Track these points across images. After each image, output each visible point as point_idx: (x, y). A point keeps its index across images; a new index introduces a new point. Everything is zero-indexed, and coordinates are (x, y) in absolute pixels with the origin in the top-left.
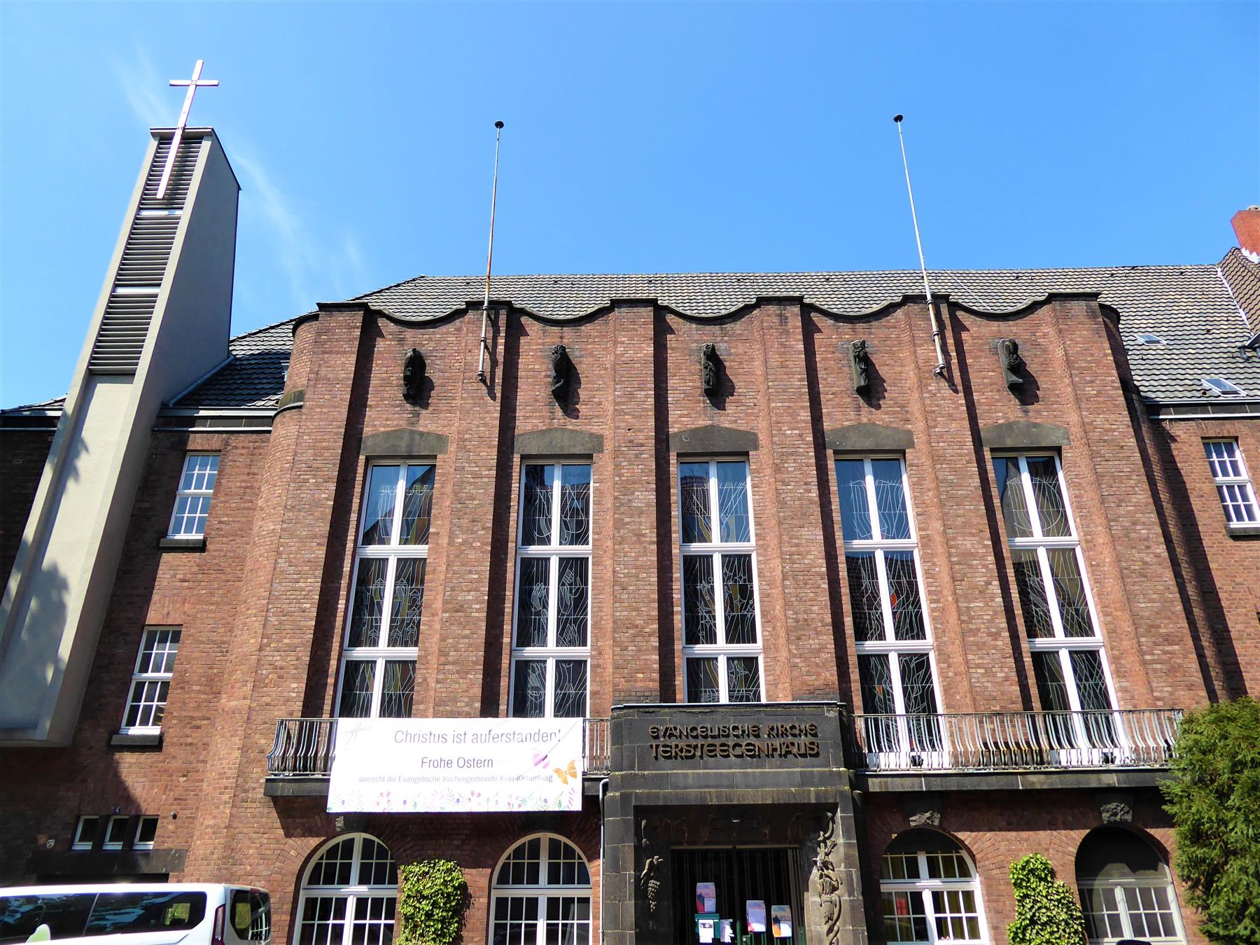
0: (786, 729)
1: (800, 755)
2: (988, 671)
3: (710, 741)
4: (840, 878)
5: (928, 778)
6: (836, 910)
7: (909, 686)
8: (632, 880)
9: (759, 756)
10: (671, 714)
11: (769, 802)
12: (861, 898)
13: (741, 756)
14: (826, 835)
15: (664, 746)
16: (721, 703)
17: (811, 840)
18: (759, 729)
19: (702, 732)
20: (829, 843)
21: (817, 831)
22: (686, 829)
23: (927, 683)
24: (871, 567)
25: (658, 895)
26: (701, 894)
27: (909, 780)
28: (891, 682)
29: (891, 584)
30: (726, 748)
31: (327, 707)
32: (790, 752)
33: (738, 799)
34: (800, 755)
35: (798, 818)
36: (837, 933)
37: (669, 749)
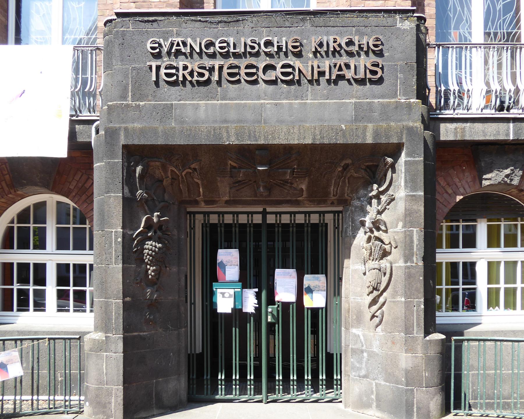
0: (340, 45)
1: (356, 80)
3: (232, 61)
4: (395, 240)
5: (519, 124)
6: (385, 280)
7: (492, 31)
8: (120, 240)
9: (299, 82)
11: (309, 141)
12: (421, 263)
13: (273, 82)
14: (381, 189)
17: (359, 199)
18: (301, 45)
19: (221, 48)
20: (383, 198)
21: (368, 184)
22: (199, 182)
23: (513, 28)
26: (222, 262)
28: (470, 27)
30: (254, 70)
32: (341, 77)
33: (266, 138)
34: (355, 80)
35: (346, 167)
36: (384, 304)
37: (173, 71)
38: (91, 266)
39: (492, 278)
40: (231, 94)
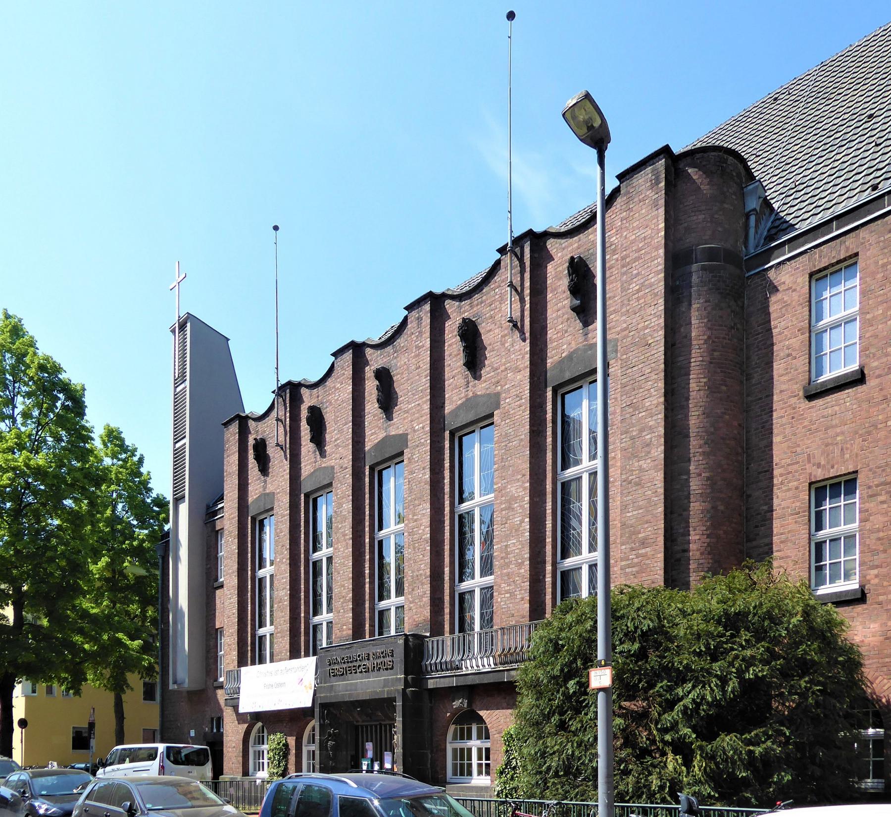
3: (350, 665)
10: (335, 651)
13: (361, 672)
16: (392, 635)
25: (334, 748)
27: (447, 679)
38: (314, 752)
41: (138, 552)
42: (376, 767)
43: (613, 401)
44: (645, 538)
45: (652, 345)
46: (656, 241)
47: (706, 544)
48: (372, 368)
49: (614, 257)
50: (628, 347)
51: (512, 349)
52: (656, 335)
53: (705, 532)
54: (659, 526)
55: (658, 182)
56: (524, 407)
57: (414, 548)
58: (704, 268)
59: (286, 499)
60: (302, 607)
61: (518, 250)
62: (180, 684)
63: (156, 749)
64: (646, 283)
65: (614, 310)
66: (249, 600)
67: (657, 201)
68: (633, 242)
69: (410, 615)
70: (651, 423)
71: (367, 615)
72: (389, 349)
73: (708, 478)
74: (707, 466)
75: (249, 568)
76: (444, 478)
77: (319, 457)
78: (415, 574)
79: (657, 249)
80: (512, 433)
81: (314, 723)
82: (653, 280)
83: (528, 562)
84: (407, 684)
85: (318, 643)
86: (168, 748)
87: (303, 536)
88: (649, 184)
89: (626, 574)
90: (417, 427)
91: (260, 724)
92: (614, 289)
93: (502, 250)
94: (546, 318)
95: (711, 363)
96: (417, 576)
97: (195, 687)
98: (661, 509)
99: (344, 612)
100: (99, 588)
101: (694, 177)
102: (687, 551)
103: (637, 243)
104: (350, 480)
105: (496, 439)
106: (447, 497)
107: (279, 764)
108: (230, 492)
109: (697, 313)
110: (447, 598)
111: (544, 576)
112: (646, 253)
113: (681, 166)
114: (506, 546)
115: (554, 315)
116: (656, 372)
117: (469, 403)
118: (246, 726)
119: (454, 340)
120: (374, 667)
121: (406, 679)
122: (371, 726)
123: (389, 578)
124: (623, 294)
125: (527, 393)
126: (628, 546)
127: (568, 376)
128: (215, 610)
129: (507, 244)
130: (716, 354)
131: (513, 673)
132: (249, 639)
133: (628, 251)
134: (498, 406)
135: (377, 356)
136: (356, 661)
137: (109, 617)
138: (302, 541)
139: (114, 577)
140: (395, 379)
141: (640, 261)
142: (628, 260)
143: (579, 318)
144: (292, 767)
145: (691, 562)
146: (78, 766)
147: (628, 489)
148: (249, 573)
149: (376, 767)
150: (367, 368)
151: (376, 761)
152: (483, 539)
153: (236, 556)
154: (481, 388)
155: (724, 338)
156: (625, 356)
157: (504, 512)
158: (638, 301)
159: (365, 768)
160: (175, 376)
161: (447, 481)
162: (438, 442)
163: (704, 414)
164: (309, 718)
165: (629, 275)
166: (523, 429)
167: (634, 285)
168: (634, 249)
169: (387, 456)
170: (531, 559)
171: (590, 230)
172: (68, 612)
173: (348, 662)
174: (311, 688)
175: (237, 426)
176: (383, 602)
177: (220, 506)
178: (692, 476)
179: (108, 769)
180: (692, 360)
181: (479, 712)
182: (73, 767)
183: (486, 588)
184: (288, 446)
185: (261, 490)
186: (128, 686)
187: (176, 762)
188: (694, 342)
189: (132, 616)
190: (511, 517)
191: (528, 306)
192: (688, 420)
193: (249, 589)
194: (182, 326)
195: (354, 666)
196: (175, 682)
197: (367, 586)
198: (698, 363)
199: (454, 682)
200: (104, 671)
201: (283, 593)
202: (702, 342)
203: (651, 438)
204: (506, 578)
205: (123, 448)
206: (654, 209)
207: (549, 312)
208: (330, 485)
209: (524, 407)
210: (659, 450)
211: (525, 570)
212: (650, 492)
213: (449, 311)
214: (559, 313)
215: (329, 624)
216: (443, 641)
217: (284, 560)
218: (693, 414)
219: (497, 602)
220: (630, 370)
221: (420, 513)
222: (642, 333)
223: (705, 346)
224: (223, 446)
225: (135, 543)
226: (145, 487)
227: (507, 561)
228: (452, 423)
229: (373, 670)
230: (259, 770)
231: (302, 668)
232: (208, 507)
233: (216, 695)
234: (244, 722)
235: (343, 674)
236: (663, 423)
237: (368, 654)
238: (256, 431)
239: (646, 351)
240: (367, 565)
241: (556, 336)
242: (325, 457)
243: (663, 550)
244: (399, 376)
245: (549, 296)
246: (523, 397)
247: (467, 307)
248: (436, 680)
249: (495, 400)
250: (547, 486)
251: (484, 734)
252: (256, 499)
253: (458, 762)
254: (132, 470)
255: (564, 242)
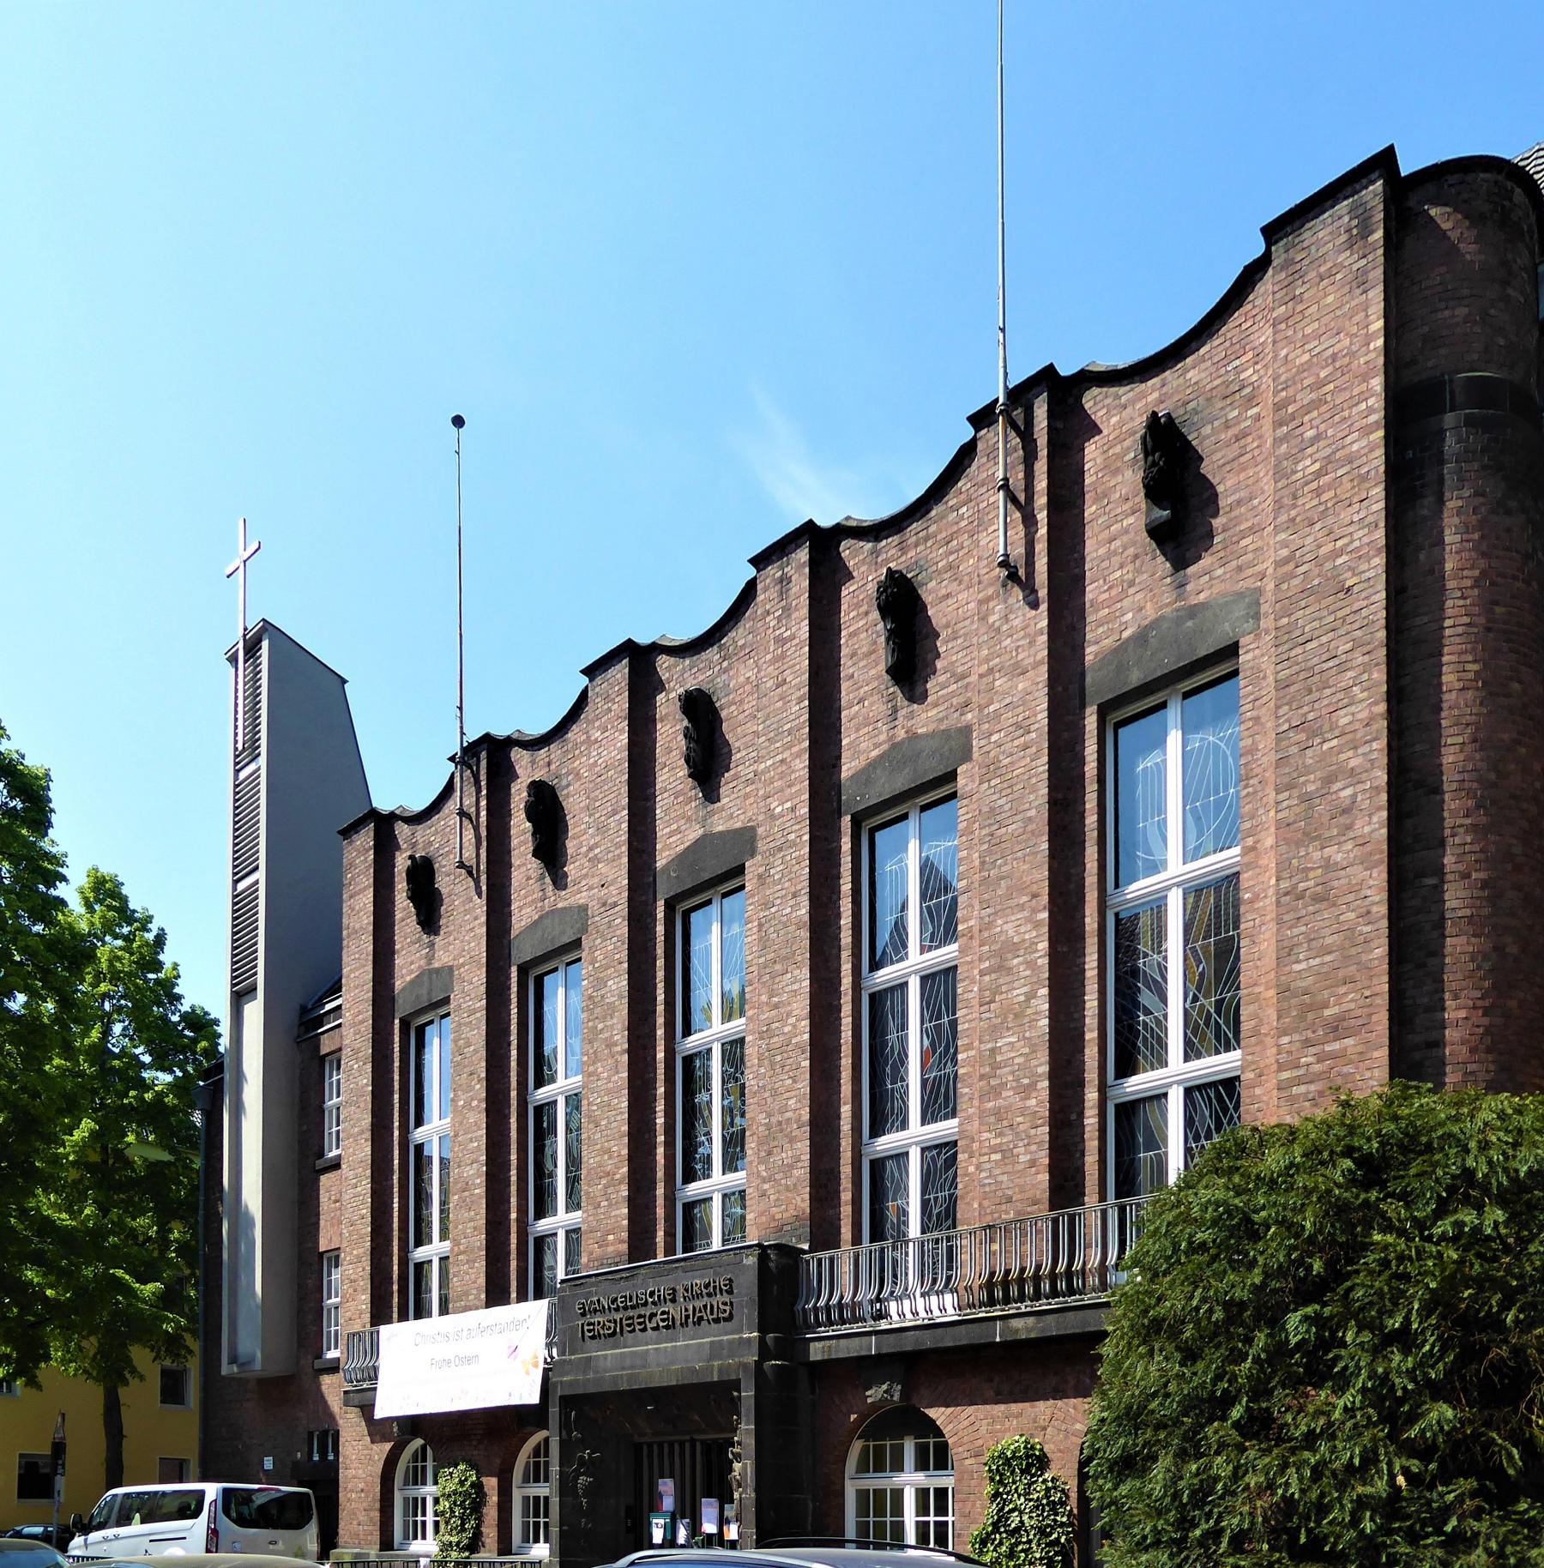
2: (1008, 1154)
3: (630, 1313)
10: (595, 1284)
12: (753, 1495)
13: (656, 1328)
15: (589, 1324)
24: (903, 1010)
25: (589, 1491)
27: (856, 1340)
29: (924, 1031)
31: (846, 1232)
38: (546, 1498)
39: (922, 1509)
40: (630, 1342)
41: (154, 1114)
42: (682, 1536)
43: (1251, 724)
44: (1341, 1018)
45: (1356, 589)
46: (1362, 361)
47: (1481, 1030)
48: (673, 695)
49: (1250, 413)
50: (1294, 600)
51: (1005, 628)
52: (1364, 567)
53: (1479, 1003)
54: (1377, 989)
55: (1365, 230)
56: (1034, 749)
57: (772, 1065)
58: (1470, 422)
59: (479, 978)
60: (514, 1200)
61: (1018, 414)
62: (243, 1364)
63: (201, 1494)
64: (1338, 455)
65: (1250, 528)
66: (396, 1190)
67: (1366, 273)
68: (1305, 368)
69: (762, 1207)
70: (1353, 763)
71: (660, 1212)
72: (712, 654)
73: (1485, 884)
74: (1482, 856)
75: (396, 1124)
76: (838, 916)
77: (551, 888)
78: (774, 1120)
79: (1365, 378)
80: (1007, 807)
81: (550, 1435)
82: (1355, 447)
83: (1046, 1083)
84: (764, 1352)
85: (546, 1273)
86: (225, 1491)
87: (514, 1053)
88: (1344, 238)
89: (1292, 1099)
90: (779, 810)
91: (419, 1442)
92: (1250, 481)
93: (981, 419)
94: (1083, 558)
95: (1489, 630)
96: (780, 1123)
97: (278, 1369)
98: (1379, 951)
99: (610, 1205)
100: (75, 1183)
101: (1445, 226)
102: (1439, 1043)
103: (1315, 370)
104: (624, 930)
105: (962, 826)
106: (846, 955)
107: (463, 1524)
108: (356, 969)
109: (1456, 520)
110: (846, 1170)
111: (1081, 1115)
112: (1339, 389)
113: (1411, 203)
114: (993, 1051)
115: (1102, 551)
116: (1366, 649)
117: (896, 755)
118: (388, 1446)
119: (861, 623)
120: (687, 1317)
121: (762, 1340)
122: (671, 1445)
123: (708, 1134)
124: (1280, 485)
125: (1042, 718)
126: (1296, 1037)
127: (1135, 678)
128: (318, 1214)
129: (997, 400)
130: (1498, 610)
131: (1017, 1323)
132: (396, 1268)
133: (1291, 391)
134: (966, 756)
135: (684, 671)
136: (646, 1303)
137: (98, 1234)
138: (514, 1064)
139: (105, 1162)
140: (723, 714)
141: (1323, 409)
142: (1290, 410)
143: (1164, 554)
144: (490, 1533)
145: (1448, 1069)
146: (27, 1530)
147: (1296, 909)
148: (396, 1133)
149: (682, 1536)
150: (661, 698)
151: (683, 1517)
152: (926, 1042)
153: (369, 1098)
154: (925, 719)
155: (1515, 578)
156: (1285, 621)
157: (987, 978)
158: (1318, 496)
159: (658, 1536)
160: (236, 749)
161: (846, 921)
162: (826, 839)
163: (1475, 741)
164: (530, 1429)
165: (1294, 442)
166: (1032, 797)
167: (1308, 462)
168: (1306, 382)
169: (706, 876)
170: (1053, 1076)
171: (1189, 360)
172: (13, 1220)
173: (625, 1308)
174: (536, 1365)
175: (372, 834)
176: (693, 1185)
177: (328, 1007)
178: (1449, 877)
179: (95, 1536)
180: (1448, 623)
181: (927, 1411)
182: (19, 1535)
183: (936, 1147)
184: (483, 867)
185: (422, 962)
186: (134, 1371)
187: (242, 1522)
188: (1450, 584)
189: (141, 1238)
190: (1004, 988)
191: (1043, 531)
192: (1440, 755)
193: (396, 1167)
194: (252, 648)
195: (640, 1316)
196: (233, 1360)
197: (660, 1151)
198: (1460, 630)
199: (873, 1347)
200: (84, 1344)
201: (473, 1173)
202: (1469, 583)
203: (1354, 795)
204: (992, 1119)
205: (124, 913)
206: (1358, 291)
207: (1090, 545)
208: (576, 944)
209: (1034, 749)
210: (1375, 819)
211: (1040, 1100)
212: (1352, 915)
213: (851, 564)
214: (1117, 543)
215: (573, 1235)
216: (832, 1260)
217: (475, 1103)
218: (1449, 741)
219: (966, 1175)
220: (1299, 650)
221: (787, 989)
222: (1328, 565)
223: (1476, 592)
224: (341, 875)
225: (148, 1096)
226: (167, 991)
227: (993, 1082)
228: (855, 797)
229: (684, 1324)
230: (415, 1538)
231: (517, 1324)
232: (304, 1010)
233: (319, 1385)
234: (385, 1439)
235: (614, 1334)
236: (1385, 761)
237: (674, 1290)
238: (410, 843)
239: (1342, 603)
240: (660, 1107)
241: (1106, 595)
242: (565, 887)
243: (1386, 1041)
244: (733, 708)
245: (1090, 511)
246: (1033, 728)
247: (893, 551)
248: (828, 1343)
249: (959, 744)
250: (1087, 920)
251: (936, 1456)
252: (412, 982)
253: (871, 1519)
254: (143, 957)
255: (1125, 393)
